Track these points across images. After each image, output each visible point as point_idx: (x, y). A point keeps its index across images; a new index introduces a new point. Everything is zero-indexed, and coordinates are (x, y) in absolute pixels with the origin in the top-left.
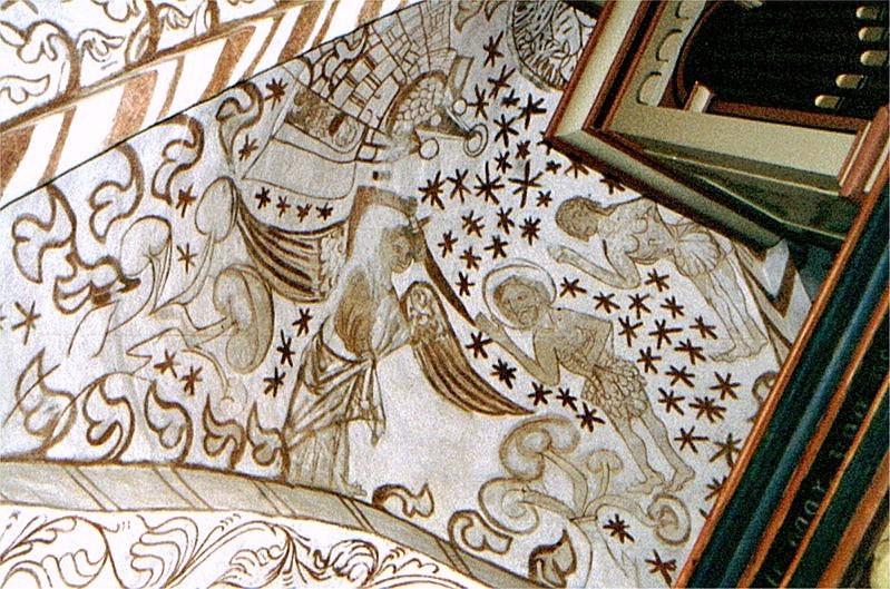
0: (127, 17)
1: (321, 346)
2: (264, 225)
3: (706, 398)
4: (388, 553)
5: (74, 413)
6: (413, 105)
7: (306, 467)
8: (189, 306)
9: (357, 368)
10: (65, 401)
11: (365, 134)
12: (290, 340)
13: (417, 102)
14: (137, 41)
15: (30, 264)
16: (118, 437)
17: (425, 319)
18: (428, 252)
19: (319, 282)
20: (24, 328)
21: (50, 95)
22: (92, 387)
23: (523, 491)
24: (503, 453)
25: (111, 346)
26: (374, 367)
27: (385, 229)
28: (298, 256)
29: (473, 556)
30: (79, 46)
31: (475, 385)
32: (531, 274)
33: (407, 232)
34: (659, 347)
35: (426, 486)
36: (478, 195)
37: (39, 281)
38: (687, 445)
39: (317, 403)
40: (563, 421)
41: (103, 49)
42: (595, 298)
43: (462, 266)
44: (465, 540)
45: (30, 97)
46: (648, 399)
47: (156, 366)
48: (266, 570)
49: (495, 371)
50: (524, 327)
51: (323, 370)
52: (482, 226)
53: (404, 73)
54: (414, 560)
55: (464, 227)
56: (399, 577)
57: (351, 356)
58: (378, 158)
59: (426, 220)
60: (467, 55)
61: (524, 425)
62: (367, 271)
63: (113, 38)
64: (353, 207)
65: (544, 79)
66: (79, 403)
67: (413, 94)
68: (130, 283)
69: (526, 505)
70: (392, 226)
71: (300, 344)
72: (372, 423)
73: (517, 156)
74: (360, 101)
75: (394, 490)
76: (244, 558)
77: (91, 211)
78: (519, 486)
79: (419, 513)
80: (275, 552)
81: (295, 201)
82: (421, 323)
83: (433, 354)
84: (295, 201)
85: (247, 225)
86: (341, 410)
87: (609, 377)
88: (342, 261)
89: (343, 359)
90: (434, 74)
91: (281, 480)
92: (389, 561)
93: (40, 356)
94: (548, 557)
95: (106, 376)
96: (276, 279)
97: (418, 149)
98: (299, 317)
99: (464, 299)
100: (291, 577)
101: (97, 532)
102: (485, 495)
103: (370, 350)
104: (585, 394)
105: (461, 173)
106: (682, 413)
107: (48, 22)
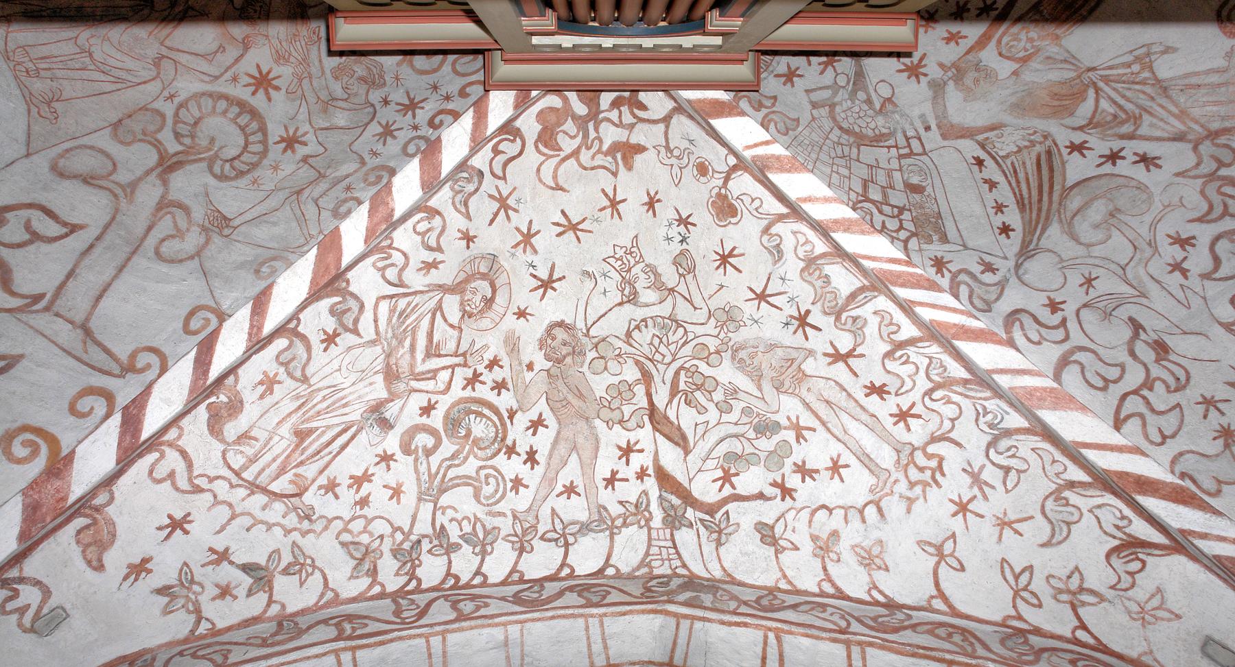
0: (954, 403)
1: (1092, 124)
2: (1022, 218)
8: (1123, 263)
9: (1101, 84)
12: (1101, 156)
13: (859, 121)
15: (1173, 418)
18: (968, 53)
20: (1219, 405)
21: (1047, 446)
25: (1192, 326)
26: (1093, 69)
28: (1027, 174)
33: (959, 77)
37: (1178, 405)
39: (1150, 114)
41: (989, 417)
47: (1186, 278)
51: (1115, 116)
57: (1091, 93)
59: (941, 65)
62: (1009, 103)
64: (962, 137)
67: (857, 129)
68: (1137, 327)
70: (960, 95)
71: (1100, 145)
72: (1153, 57)
77: (1111, 385)
81: (990, 198)
84: (990, 198)
85: (1033, 235)
86: (1148, 89)
88: (1008, 130)
89: (1097, 101)
90: (834, 120)
95: (1221, 324)
97: (889, 100)
98: (1076, 153)
103: (1079, 77)
107: (987, 456)
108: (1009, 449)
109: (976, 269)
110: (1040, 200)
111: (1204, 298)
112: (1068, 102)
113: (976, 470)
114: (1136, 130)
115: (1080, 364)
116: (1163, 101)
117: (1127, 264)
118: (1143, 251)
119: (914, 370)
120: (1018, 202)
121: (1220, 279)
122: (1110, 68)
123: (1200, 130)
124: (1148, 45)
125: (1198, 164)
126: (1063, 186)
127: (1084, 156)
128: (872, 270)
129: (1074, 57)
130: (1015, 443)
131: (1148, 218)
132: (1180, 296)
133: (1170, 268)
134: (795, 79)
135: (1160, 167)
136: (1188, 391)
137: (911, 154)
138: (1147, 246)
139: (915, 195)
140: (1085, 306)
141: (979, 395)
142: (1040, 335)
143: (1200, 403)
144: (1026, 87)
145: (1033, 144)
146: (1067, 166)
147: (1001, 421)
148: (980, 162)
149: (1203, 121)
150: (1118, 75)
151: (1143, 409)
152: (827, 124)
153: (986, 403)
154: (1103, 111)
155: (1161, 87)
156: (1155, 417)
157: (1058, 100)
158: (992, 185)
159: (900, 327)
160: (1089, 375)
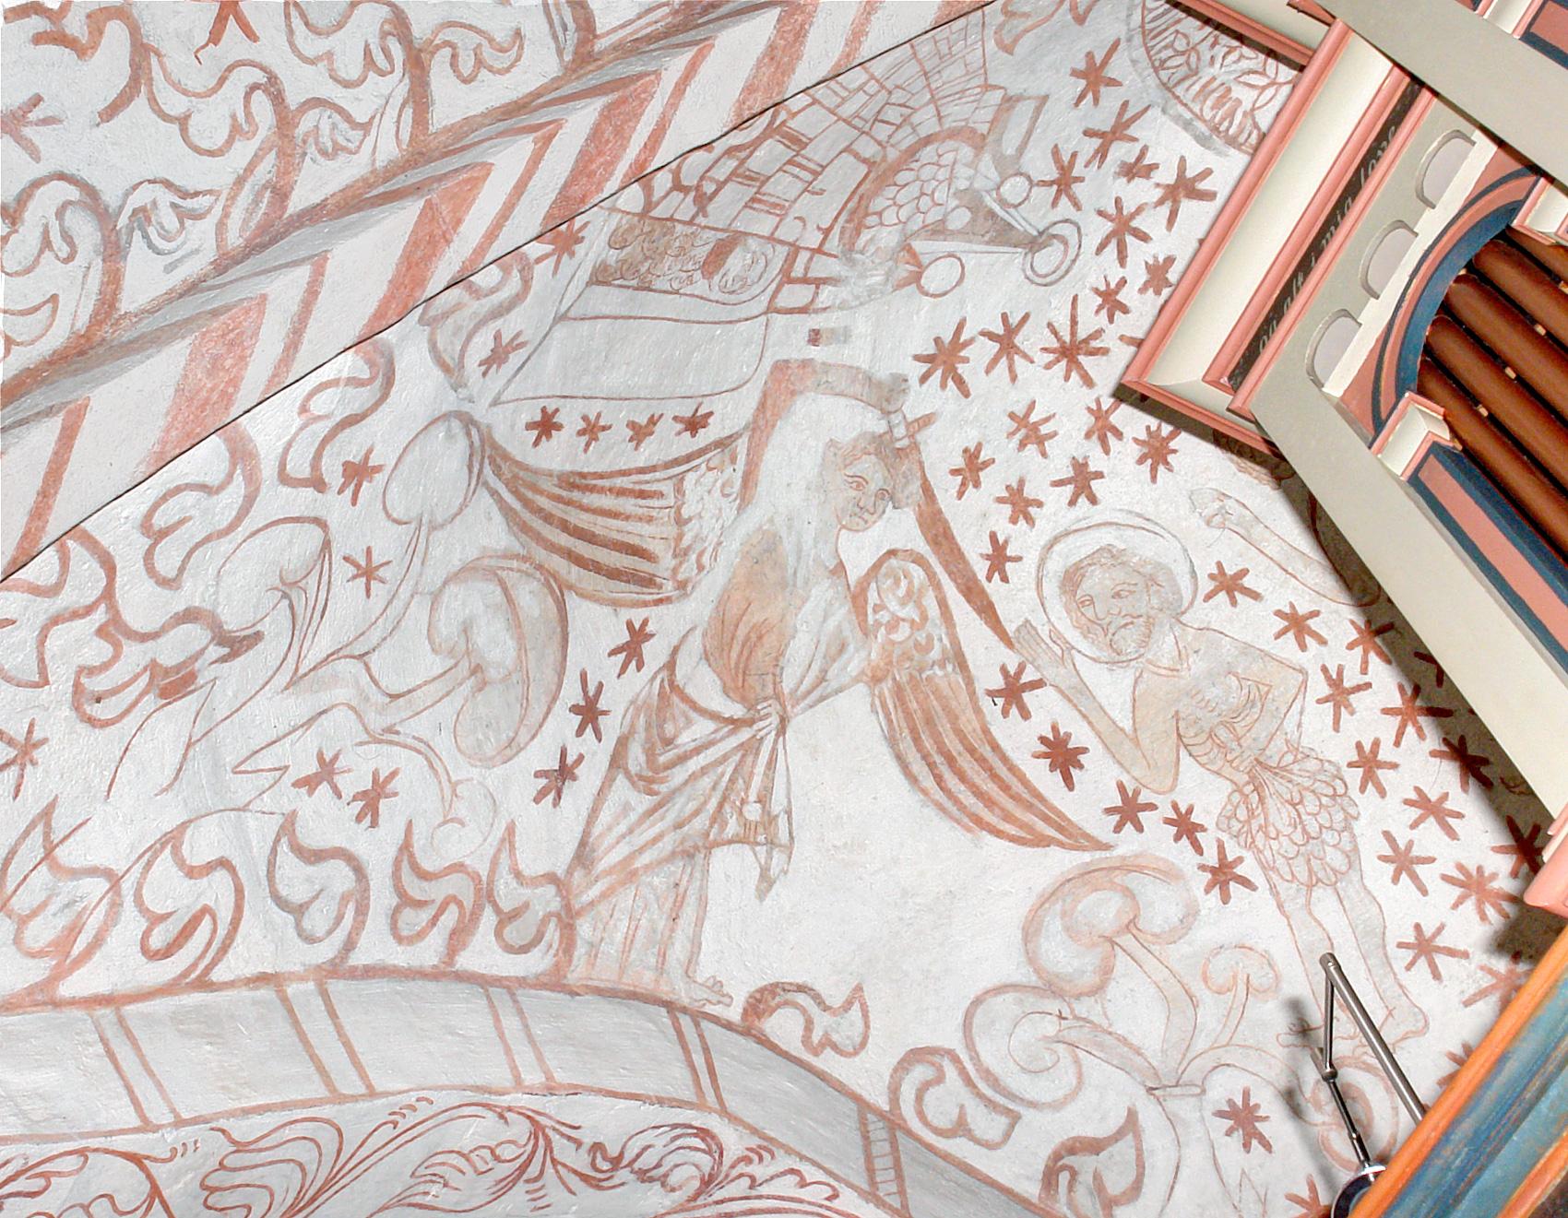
0: (230, 142)
1: (671, 689)
3: (1480, 869)
4: (741, 1152)
5: (116, 906)
6: (901, 198)
7: (611, 950)
8: (374, 659)
9: (745, 734)
10: (100, 886)
11: (790, 260)
13: (914, 190)
14: (245, 196)
16: (207, 936)
17: (903, 633)
18: (927, 489)
19: (674, 562)
21: (56, 339)
22: (154, 852)
23: (1061, 1017)
24: (1031, 931)
26: (782, 730)
27: (832, 443)
28: (627, 518)
29: (930, 1148)
30: (123, 221)
31: (995, 777)
32: (1146, 548)
34: (1397, 743)
35: (859, 988)
36: (1048, 366)
38: (1422, 962)
40: (1169, 874)
41: (171, 221)
42: (1279, 613)
43: (1000, 520)
44: (921, 1115)
45: (14, 348)
46: (1356, 849)
47: (297, 784)
48: (489, 1179)
49: (1044, 749)
50: (1117, 660)
51: (668, 742)
52: (1053, 435)
53: (879, 143)
54: (792, 1171)
55: (1012, 434)
56: (759, 1197)
57: (737, 710)
58: (819, 304)
59: (926, 421)
60: (1031, 92)
61: (1086, 873)
62: (783, 533)
63: (196, 194)
64: (762, 406)
65: (1216, 129)
66: (127, 886)
67: (903, 177)
68: (236, 644)
69: (1061, 1048)
70: (846, 436)
72: (762, 850)
73: (1143, 290)
74: (775, 205)
75: (789, 996)
76: (443, 1164)
77: (147, 542)
78: (1054, 1006)
79: (835, 1047)
80: (507, 1152)
81: (618, 417)
82: (895, 637)
83: (914, 705)
84: (618, 417)
86: (700, 823)
87: (1282, 790)
88: (729, 511)
89: (714, 716)
90: (953, 134)
91: (554, 982)
92: (742, 1168)
93: (47, 814)
94: (1085, 1163)
95: (184, 826)
96: (575, 569)
97: (916, 278)
98: (625, 637)
99: (994, 589)
100: (543, 1187)
101: (132, 1167)
102: (978, 1020)
103: (778, 696)
104: (1227, 818)
105: (1014, 320)
106: (1424, 892)
107: (61, 176)
108: (67, 238)
109: (510, 325)
110: (565, 526)
111: (244, 809)
112: (734, 655)
113: (28, 132)
114: (627, 773)
115: (221, 488)
116: (667, 845)
117: (368, 669)
118: (382, 711)
119: (343, 74)
120: (583, 475)
121: (274, 851)
122: (771, 763)
123: (585, 898)
124: (789, 849)
125: (518, 875)
126: (570, 587)
127: (613, 653)
128: (657, 73)
129: (822, 699)
130: (80, 260)
131: (443, 744)
132: (266, 760)
133: (328, 757)
134: (1082, 83)
135: (537, 800)
136: (66, 711)
137: (787, 278)
138: (389, 721)
139: (708, 248)
140: (327, 545)
141: (237, 214)
142: (320, 418)
143: (30, 732)
144: (800, 582)
145: (681, 554)
146: (607, 610)
147: (151, 245)
148: (694, 424)
149: (603, 909)
150: (751, 774)
151: (68, 599)
152: (956, 113)
153: (209, 224)
154: (689, 722)
155: (696, 848)
156: (42, 619)
157: (747, 638)
158: (640, 433)
159: (465, 81)
160: (189, 498)
